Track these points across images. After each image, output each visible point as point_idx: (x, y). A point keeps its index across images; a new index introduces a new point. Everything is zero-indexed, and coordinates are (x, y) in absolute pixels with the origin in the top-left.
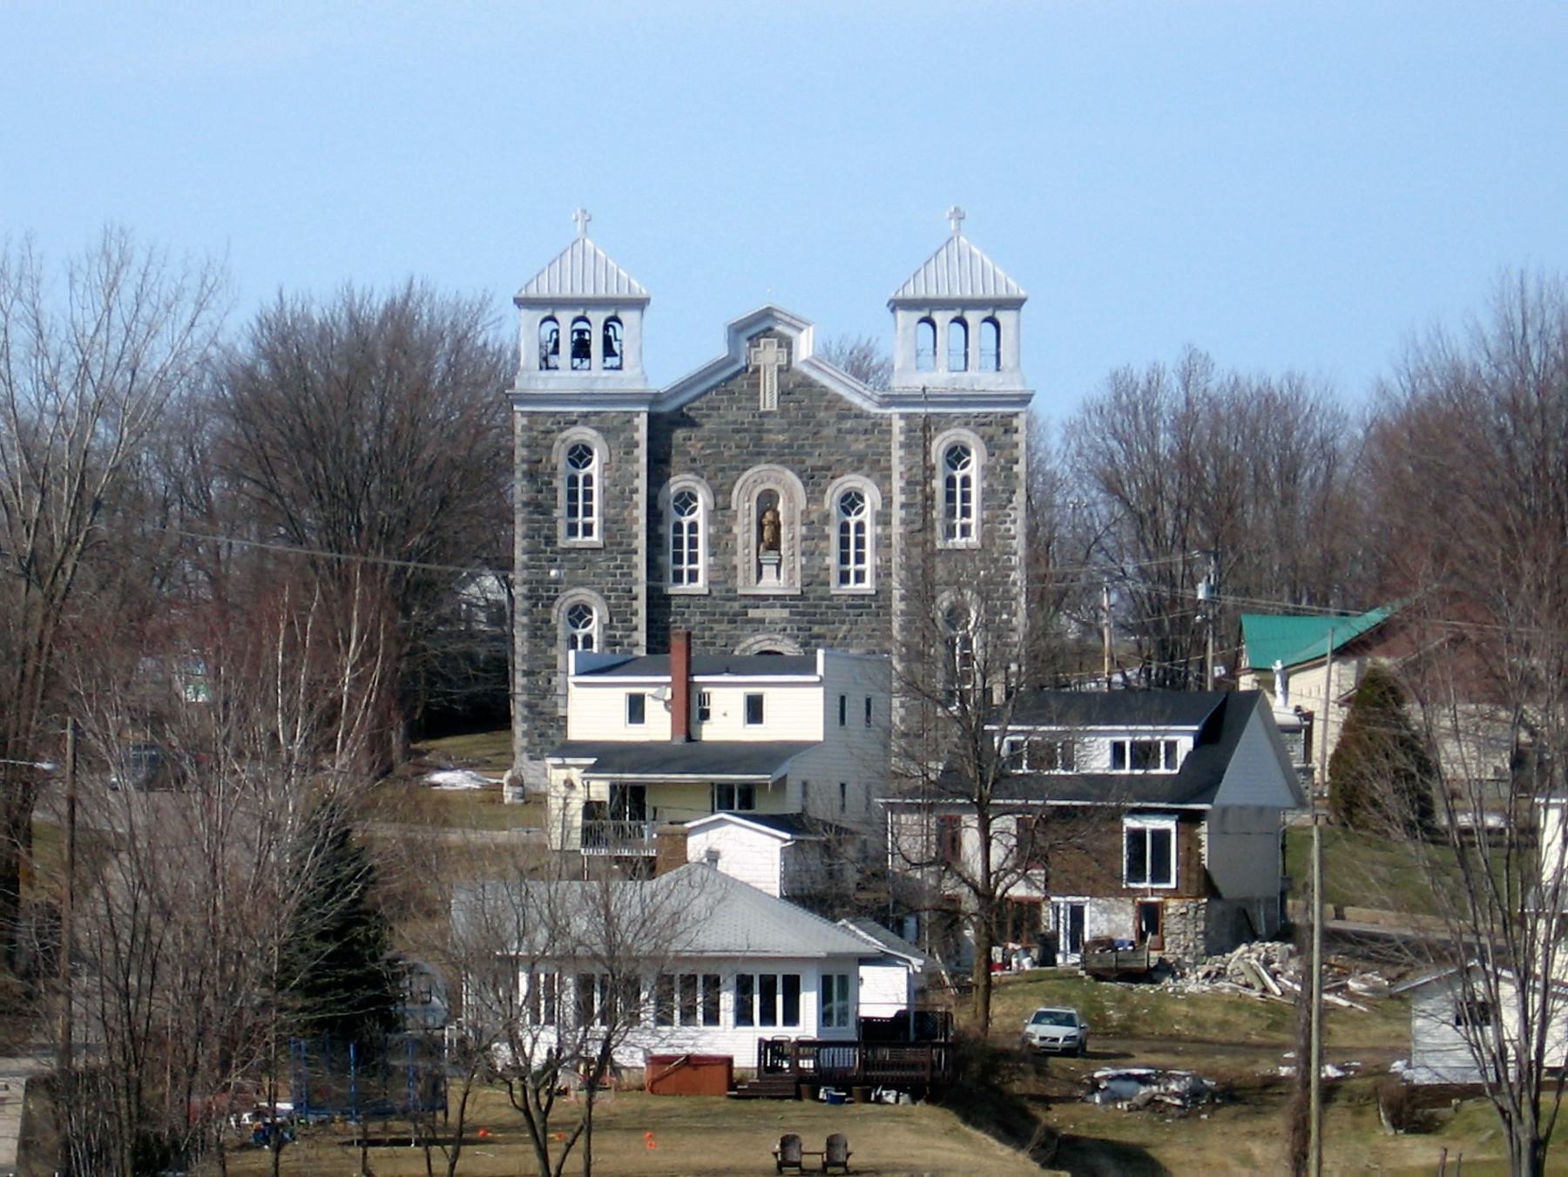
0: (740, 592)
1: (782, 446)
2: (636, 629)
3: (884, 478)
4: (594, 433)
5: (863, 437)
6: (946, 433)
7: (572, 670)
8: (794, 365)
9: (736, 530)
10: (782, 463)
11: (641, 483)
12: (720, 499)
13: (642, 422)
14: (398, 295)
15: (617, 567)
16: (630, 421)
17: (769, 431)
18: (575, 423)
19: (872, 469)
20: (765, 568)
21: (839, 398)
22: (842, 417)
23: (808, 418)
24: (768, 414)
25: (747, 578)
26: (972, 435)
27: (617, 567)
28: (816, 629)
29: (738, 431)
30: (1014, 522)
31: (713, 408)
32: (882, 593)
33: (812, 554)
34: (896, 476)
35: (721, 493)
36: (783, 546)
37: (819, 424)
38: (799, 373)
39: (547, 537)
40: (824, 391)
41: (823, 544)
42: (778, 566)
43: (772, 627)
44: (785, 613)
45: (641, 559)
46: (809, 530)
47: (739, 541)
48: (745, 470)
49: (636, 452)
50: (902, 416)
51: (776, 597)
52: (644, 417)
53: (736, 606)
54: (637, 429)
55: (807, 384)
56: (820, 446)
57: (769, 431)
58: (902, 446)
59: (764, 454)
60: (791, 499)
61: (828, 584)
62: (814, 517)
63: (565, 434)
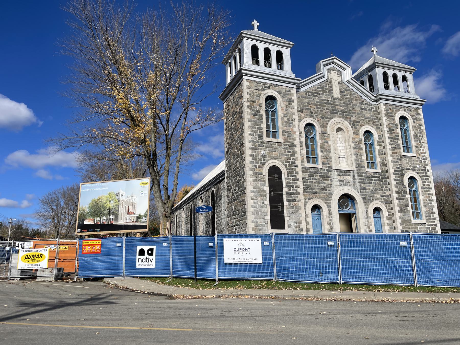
3: (379, 126)
4: (277, 94)
9: (329, 142)
14: (43, 212)
17: (337, 105)
18: (269, 88)
19: (373, 124)
22: (361, 104)
23: (350, 102)
24: (336, 99)
30: (424, 147)
31: (317, 93)
35: (324, 126)
37: (354, 105)
39: (259, 135)
46: (355, 145)
47: (332, 147)
48: (331, 119)
54: (293, 95)
57: (337, 105)
58: (386, 115)
59: (337, 114)
63: (265, 92)
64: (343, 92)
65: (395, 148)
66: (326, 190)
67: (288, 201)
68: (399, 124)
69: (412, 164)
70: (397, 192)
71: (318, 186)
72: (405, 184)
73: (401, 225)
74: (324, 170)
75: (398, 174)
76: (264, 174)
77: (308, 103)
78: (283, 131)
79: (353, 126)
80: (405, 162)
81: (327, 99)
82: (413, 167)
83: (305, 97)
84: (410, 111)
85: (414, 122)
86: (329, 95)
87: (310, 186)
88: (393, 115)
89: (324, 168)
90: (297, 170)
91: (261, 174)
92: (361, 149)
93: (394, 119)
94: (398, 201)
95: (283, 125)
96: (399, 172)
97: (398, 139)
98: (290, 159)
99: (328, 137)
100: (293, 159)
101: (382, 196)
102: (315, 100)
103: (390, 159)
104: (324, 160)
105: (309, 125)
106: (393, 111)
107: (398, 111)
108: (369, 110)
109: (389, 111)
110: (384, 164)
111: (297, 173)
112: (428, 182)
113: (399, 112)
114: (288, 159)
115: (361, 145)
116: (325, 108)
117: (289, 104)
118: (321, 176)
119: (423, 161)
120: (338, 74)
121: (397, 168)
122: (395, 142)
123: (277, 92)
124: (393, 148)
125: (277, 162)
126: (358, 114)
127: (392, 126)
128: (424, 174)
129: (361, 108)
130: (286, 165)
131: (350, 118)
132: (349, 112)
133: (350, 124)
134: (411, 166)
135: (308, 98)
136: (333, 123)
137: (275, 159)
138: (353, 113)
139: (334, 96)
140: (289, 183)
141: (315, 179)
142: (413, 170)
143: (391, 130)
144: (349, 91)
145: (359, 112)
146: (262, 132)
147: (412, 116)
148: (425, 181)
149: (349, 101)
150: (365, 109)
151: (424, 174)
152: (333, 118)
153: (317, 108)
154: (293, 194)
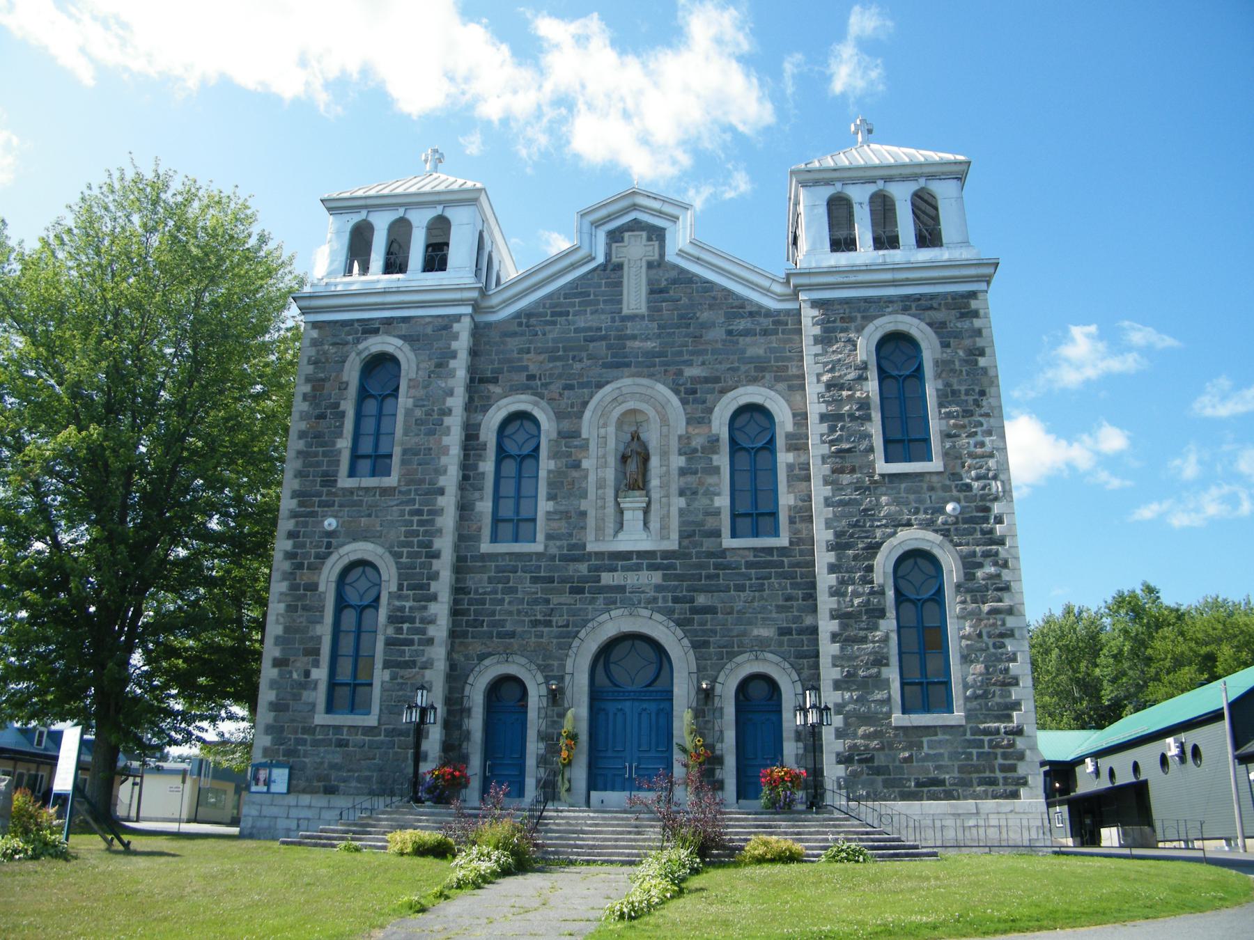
0: (590, 547)
1: (651, 354)
2: (434, 598)
4: (399, 342)
5: (761, 340)
6: (878, 322)
7: (769, 558)
8: (667, 258)
9: (585, 464)
10: (651, 376)
11: (457, 402)
12: (600, 492)
13: (463, 330)
15: (412, 513)
16: (447, 327)
17: (634, 337)
18: (376, 331)
20: (628, 515)
21: (728, 293)
23: (686, 319)
24: (632, 318)
25: (600, 529)
26: (916, 321)
27: (412, 513)
28: (701, 600)
29: (592, 340)
31: (561, 314)
32: (804, 543)
33: (695, 493)
34: (810, 381)
35: (570, 414)
36: (654, 482)
37: (703, 326)
38: (675, 267)
40: (708, 286)
41: (711, 480)
42: (646, 511)
43: (635, 597)
44: (656, 577)
45: (448, 502)
46: (689, 460)
47: (592, 478)
48: (600, 386)
49: (453, 364)
50: (815, 304)
51: (641, 554)
52: (467, 321)
53: (583, 568)
55: (685, 279)
56: (704, 352)
57: (634, 337)
59: (628, 365)
60: (665, 421)
61: (720, 536)
62: (697, 442)
67: (387, 665)
70: (834, 615)
71: (519, 612)
74: (553, 558)
76: (322, 588)
77: (521, 351)
78: (405, 452)
81: (595, 325)
83: (514, 334)
84: (931, 308)
85: (945, 345)
87: (493, 613)
89: (553, 551)
90: (435, 568)
91: (313, 587)
92: (716, 471)
95: (406, 433)
96: (855, 543)
97: (868, 418)
100: (426, 533)
101: (783, 632)
102: (550, 336)
104: (554, 525)
108: (765, 333)
110: (803, 515)
111: (435, 576)
112: (995, 564)
114: (409, 534)
116: (584, 354)
118: (535, 580)
119: (976, 485)
120: (649, 239)
123: (400, 337)
125: (369, 546)
126: (714, 352)
129: (730, 333)
130: (397, 556)
131: (680, 373)
132: (680, 353)
133: (677, 392)
135: (522, 334)
136: (609, 399)
137: (365, 539)
138: (692, 353)
139: (625, 311)
141: (513, 590)
145: (720, 346)
146: (337, 463)
148: (979, 560)
150: (746, 333)
152: (608, 383)
153: (552, 359)
154: (410, 642)
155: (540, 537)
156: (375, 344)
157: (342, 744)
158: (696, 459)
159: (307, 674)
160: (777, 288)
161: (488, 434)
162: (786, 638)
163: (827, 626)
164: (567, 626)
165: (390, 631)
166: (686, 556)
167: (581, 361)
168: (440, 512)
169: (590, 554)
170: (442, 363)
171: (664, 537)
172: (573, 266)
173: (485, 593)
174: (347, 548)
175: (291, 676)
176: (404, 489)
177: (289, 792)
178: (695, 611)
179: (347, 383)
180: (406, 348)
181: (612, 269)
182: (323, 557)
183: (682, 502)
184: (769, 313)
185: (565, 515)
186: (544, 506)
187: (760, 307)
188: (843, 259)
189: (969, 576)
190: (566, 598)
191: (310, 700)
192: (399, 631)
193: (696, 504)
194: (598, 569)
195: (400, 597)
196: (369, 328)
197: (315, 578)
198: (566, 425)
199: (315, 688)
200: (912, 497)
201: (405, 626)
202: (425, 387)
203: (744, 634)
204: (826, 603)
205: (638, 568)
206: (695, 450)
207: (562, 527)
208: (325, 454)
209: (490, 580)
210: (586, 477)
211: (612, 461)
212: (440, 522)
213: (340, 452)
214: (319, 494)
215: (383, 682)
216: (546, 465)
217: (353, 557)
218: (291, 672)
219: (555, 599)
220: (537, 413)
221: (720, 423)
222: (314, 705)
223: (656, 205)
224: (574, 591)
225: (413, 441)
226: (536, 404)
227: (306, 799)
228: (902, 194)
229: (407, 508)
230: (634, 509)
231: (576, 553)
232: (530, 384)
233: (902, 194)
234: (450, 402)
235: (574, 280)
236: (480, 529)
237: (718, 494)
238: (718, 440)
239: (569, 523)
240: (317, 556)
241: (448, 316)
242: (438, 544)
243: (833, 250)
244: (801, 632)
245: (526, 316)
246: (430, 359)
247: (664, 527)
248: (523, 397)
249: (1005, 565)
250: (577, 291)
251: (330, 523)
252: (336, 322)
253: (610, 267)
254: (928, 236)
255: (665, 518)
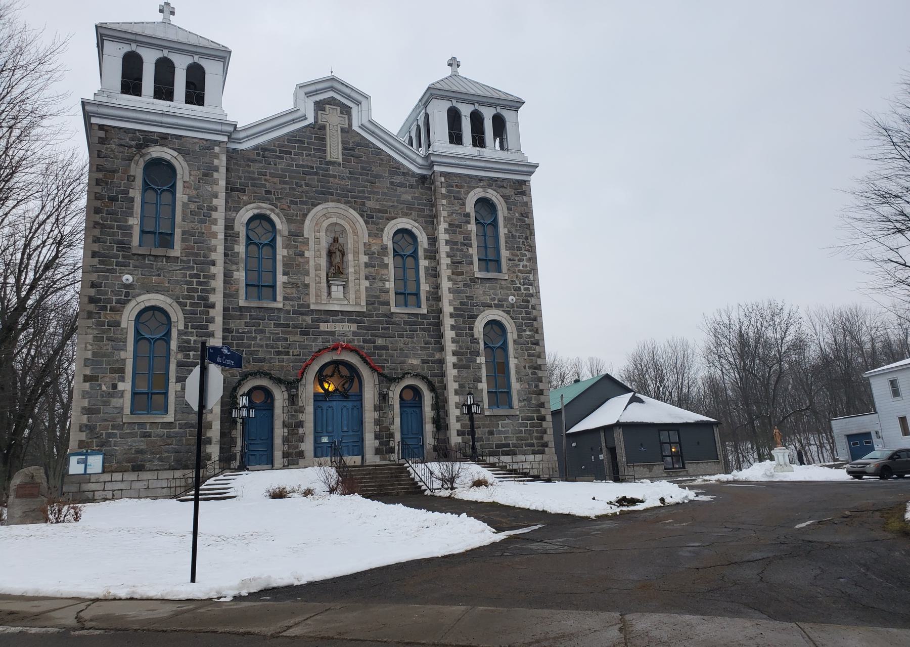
0: (312, 307)
4: (175, 154)
9: (307, 254)
10: (346, 203)
15: (191, 276)
18: (155, 142)
19: (418, 216)
24: (333, 163)
25: (318, 296)
28: (380, 342)
33: (374, 279)
35: (296, 221)
41: (384, 272)
44: (354, 327)
45: (218, 270)
47: (312, 263)
48: (314, 205)
53: (308, 319)
57: (335, 177)
59: (332, 194)
60: (355, 233)
62: (375, 248)
64: (350, 150)
65: (460, 263)
66: (287, 354)
68: (473, 214)
69: (496, 295)
70: (454, 353)
72: (476, 335)
73: (457, 421)
74: (288, 312)
75: (462, 316)
77: (260, 174)
78: (184, 233)
79: (369, 218)
80: (481, 292)
82: (499, 301)
83: (254, 161)
84: (503, 187)
85: (509, 209)
86: (315, 156)
87: (249, 346)
88: (462, 196)
89: (288, 308)
91: (117, 324)
92: (386, 266)
93: (464, 204)
94: (456, 371)
95: (183, 220)
96: (466, 314)
98: (196, 290)
99: (306, 242)
100: (203, 291)
103: (446, 285)
104: (288, 291)
105: (261, 218)
106: (461, 187)
107: (474, 188)
109: (455, 188)
110: (435, 296)
111: (212, 320)
113: (476, 190)
115: (385, 258)
116: (303, 182)
117: (206, 175)
118: (277, 325)
119: (522, 288)
120: (342, 113)
121: (462, 303)
122: (462, 250)
124: (455, 264)
125: (161, 297)
126: (384, 194)
127: (457, 219)
128: (523, 315)
129: (392, 183)
131: (364, 204)
133: (362, 216)
134: (494, 299)
136: (321, 214)
137: (157, 292)
139: (328, 158)
140: (189, 342)
141: (263, 332)
142: (498, 306)
143: (453, 228)
144: (368, 147)
147: (506, 198)
148: (524, 328)
149: (363, 168)
150: (401, 185)
151: (523, 315)
152: (319, 204)
155: (279, 298)
156: (156, 152)
157: (146, 435)
158: (375, 259)
159: (114, 386)
160: (420, 161)
161: (240, 227)
162: (426, 365)
163: (451, 359)
164: (299, 355)
165: (180, 356)
166: (371, 315)
167: (301, 186)
168: (213, 277)
169: (312, 310)
170: (208, 173)
171: (357, 304)
172: (293, 121)
173: (243, 333)
174: (140, 299)
175: (101, 389)
176: (185, 259)
177: (104, 472)
178: (376, 348)
179: (134, 177)
180: (180, 158)
181: (318, 130)
182: (124, 303)
183: (366, 283)
184: (414, 174)
185: (295, 285)
186: (281, 279)
187: (409, 170)
188: (129, 100)
189: (520, 336)
190: (298, 338)
191: (118, 405)
192: (188, 356)
193: (375, 285)
194: (319, 320)
195: (186, 334)
196: (163, 140)
197: (118, 318)
198: (293, 227)
199: (122, 396)
200: (492, 291)
201: (191, 353)
202: (196, 189)
203: (404, 362)
204: (450, 347)
205: (342, 321)
206: (374, 253)
207: (293, 292)
208: (119, 227)
209: (246, 324)
210: (308, 262)
211: (324, 253)
212: (213, 284)
213: (131, 227)
214: (117, 257)
215: (176, 392)
216: (281, 252)
217: (148, 304)
218: (100, 385)
219: (291, 338)
220: (273, 217)
221: (387, 238)
222: (122, 409)
223: (347, 91)
224: (303, 333)
225: (188, 226)
226: (272, 210)
227: (117, 476)
228: (181, 64)
229: (188, 273)
230: (338, 285)
231: (304, 310)
232: (266, 196)
233: (181, 64)
234: (215, 202)
235: (293, 132)
236: (237, 291)
237: (388, 281)
238: (387, 248)
239: (299, 291)
240: (118, 302)
241: (211, 140)
242: (212, 298)
243: (451, 142)
244: (434, 362)
245: (262, 150)
246: (199, 169)
247: (358, 298)
248: (263, 205)
249: (537, 332)
250: (294, 138)
251: (128, 278)
252: (120, 128)
253: (317, 127)
254: (195, 95)
255: (358, 292)
